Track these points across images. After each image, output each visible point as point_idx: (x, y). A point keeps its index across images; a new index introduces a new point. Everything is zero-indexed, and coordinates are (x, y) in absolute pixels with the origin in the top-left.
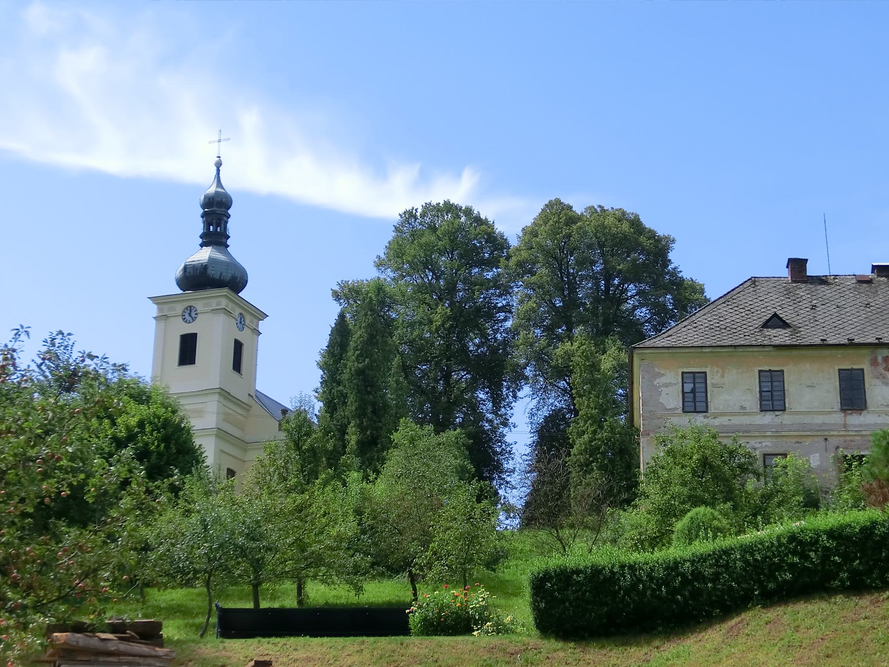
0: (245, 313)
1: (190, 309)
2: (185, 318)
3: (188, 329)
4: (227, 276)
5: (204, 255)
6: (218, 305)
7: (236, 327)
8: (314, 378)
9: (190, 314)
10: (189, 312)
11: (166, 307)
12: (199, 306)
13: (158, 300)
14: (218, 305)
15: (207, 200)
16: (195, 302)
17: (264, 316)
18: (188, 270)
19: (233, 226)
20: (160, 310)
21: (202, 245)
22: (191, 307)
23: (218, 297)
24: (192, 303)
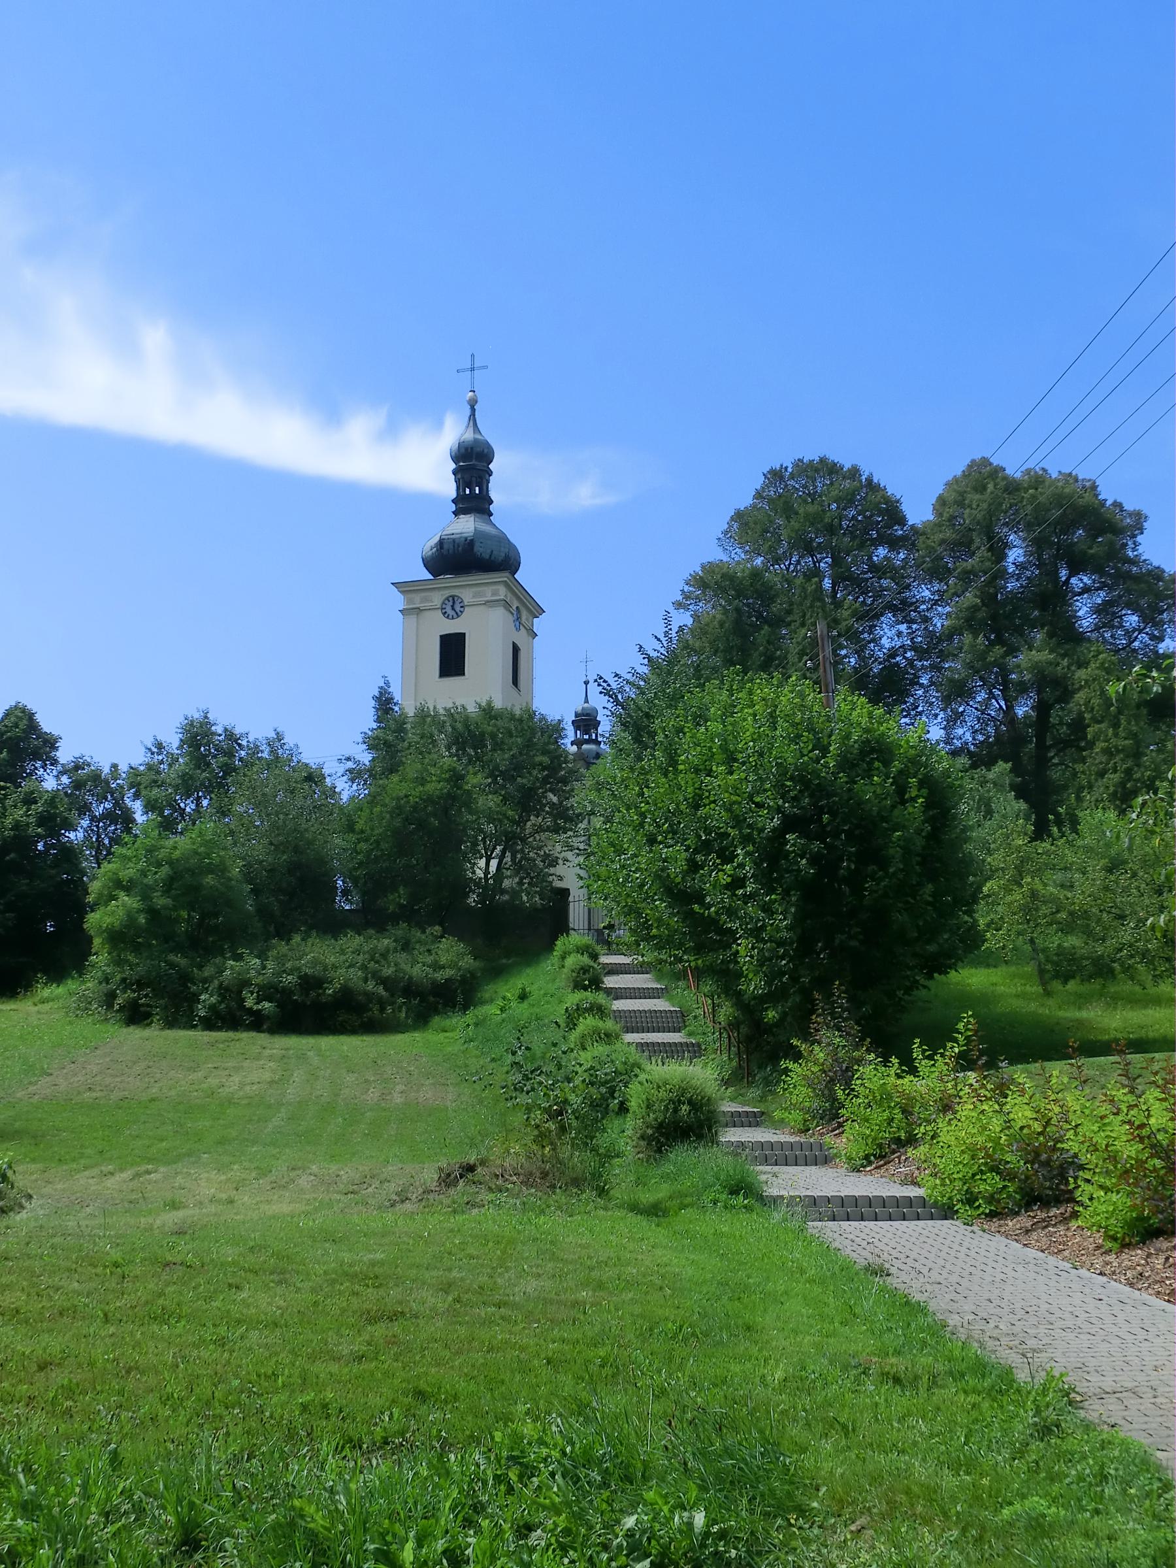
0: (521, 608)
1: (453, 599)
3: (452, 627)
4: (500, 556)
5: (467, 525)
6: (493, 595)
9: (453, 607)
10: (451, 603)
11: (417, 598)
12: (467, 596)
14: (493, 595)
15: (463, 451)
16: (461, 590)
17: (541, 612)
18: (446, 546)
19: (497, 491)
20: (409, 601)
21: (456, 513)
22: (453, 597)
23: (490, 586)
24: (455, 592)
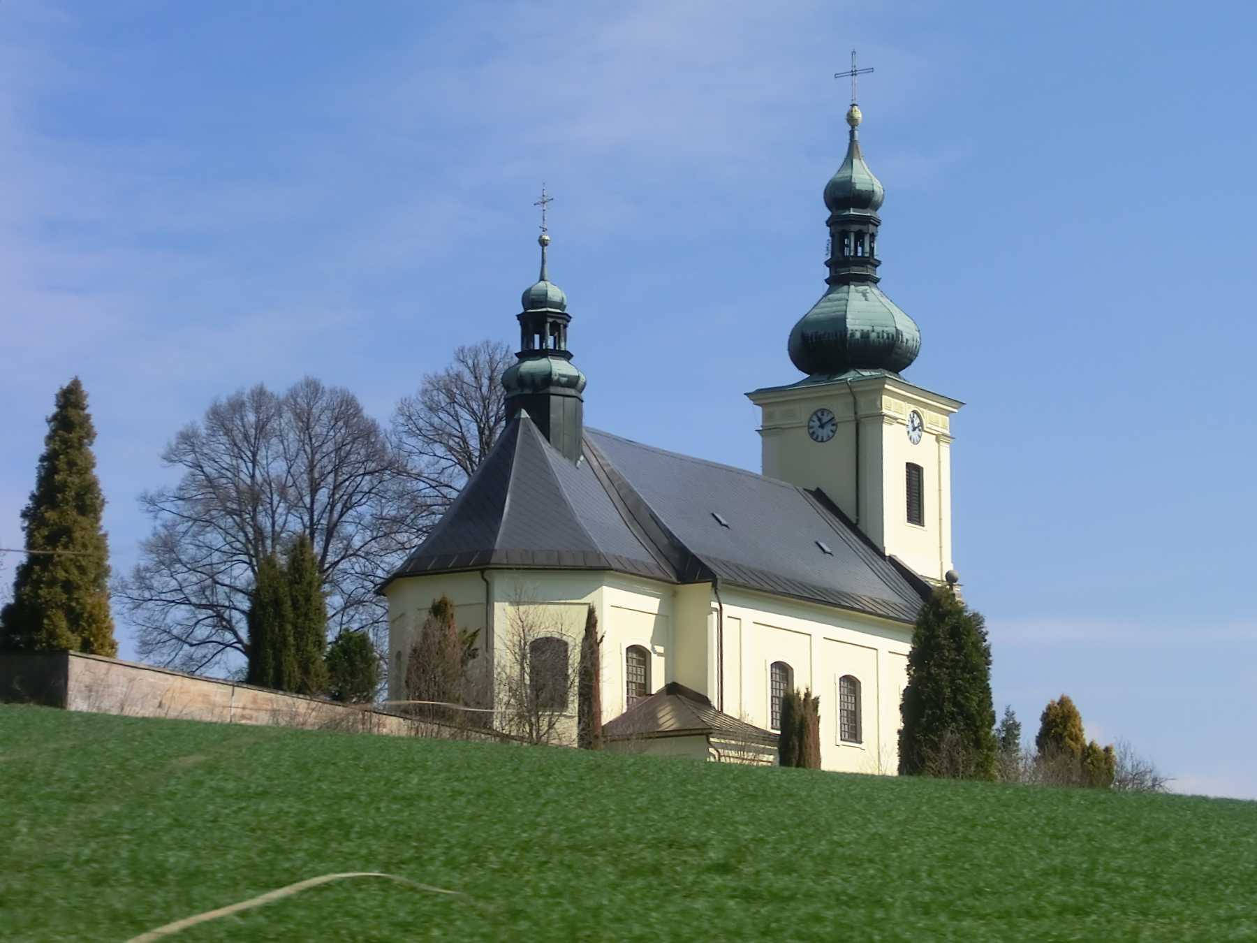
0: (920, 410)
2: (813, 433)
7: (908, 438)
8: (952, 565)
13: (759, 396)
